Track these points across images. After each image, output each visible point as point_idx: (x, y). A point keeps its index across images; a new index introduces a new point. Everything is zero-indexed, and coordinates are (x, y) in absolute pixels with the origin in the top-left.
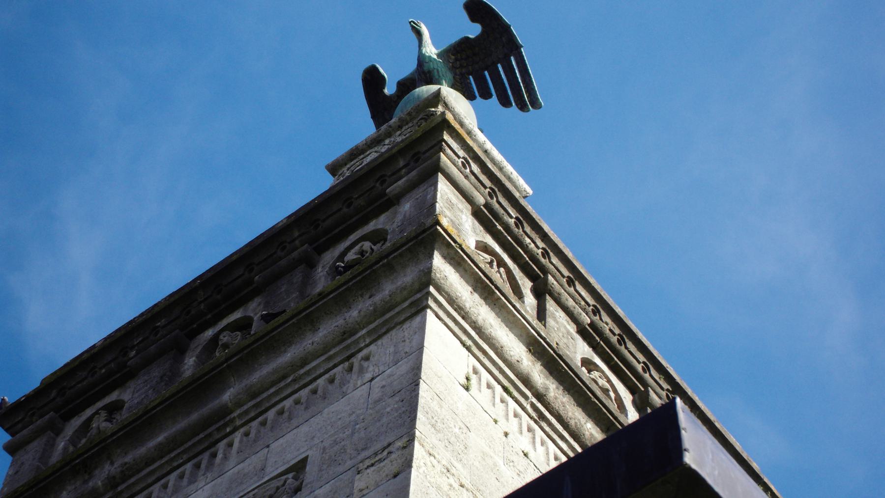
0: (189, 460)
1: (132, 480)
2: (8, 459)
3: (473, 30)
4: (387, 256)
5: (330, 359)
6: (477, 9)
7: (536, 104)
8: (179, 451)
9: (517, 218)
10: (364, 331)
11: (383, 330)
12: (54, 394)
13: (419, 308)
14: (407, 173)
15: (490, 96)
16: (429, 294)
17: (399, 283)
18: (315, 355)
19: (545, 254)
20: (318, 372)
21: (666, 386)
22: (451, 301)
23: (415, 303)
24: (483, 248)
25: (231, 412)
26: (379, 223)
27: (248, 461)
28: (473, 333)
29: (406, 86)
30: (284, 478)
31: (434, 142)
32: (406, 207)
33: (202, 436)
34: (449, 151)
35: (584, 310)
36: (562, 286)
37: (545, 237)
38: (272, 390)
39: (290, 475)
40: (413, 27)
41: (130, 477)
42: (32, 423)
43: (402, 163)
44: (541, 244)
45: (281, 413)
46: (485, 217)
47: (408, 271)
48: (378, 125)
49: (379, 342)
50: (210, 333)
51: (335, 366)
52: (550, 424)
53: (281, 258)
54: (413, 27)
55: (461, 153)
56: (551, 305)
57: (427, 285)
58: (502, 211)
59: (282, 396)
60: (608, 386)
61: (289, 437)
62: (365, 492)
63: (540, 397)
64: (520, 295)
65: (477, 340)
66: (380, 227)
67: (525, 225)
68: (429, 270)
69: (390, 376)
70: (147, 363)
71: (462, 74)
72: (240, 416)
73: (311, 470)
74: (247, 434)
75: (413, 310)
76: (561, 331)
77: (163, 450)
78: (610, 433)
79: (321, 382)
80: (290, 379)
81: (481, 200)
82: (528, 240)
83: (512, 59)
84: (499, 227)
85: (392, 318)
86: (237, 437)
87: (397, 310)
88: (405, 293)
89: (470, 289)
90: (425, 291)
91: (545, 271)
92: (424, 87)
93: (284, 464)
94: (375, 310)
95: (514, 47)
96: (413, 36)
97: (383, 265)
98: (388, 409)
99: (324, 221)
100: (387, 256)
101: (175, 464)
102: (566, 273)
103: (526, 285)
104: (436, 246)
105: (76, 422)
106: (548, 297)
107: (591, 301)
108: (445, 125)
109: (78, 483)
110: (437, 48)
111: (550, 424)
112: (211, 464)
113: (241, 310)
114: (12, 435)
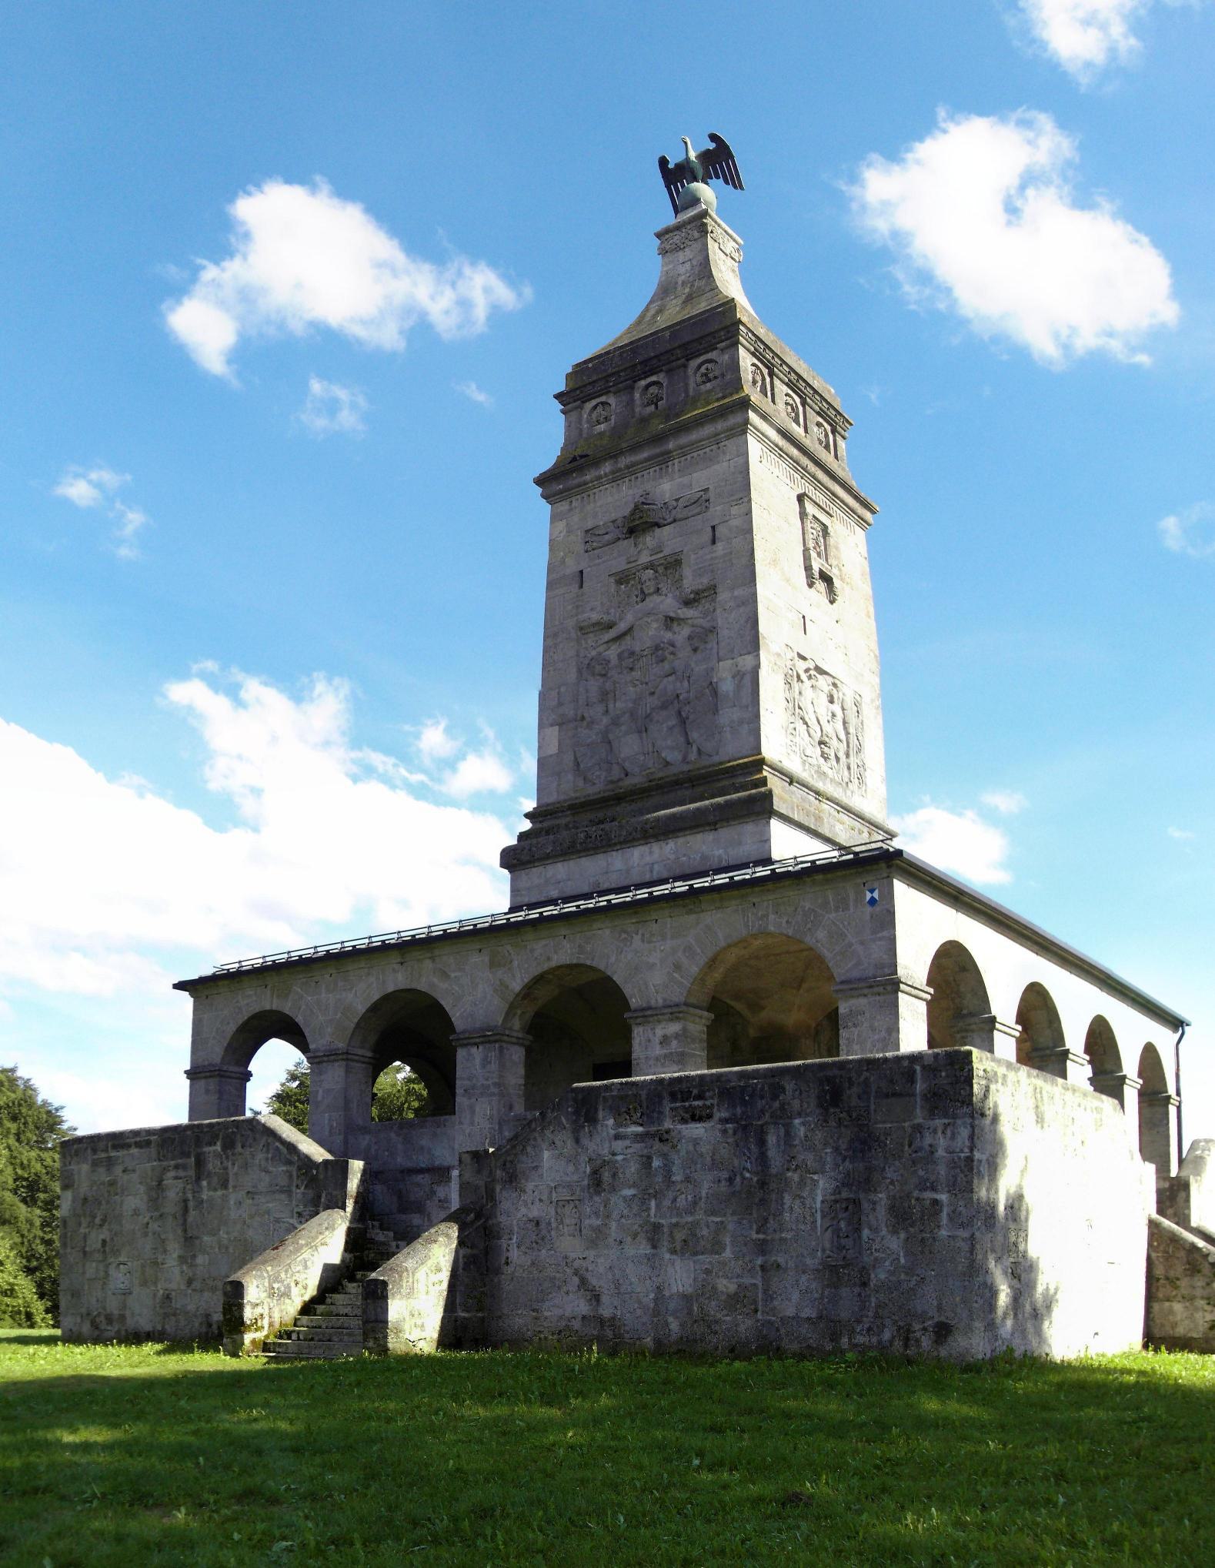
3: (712, 146)
6: (714, 138)
13: (744, 432)
23: (743, 428)
24: (753, 365)
65: (763, 437)
68: (748, 419)
77: (647, 460)
78: (539, 826)
95: (730, 155)
108: (740, 322)
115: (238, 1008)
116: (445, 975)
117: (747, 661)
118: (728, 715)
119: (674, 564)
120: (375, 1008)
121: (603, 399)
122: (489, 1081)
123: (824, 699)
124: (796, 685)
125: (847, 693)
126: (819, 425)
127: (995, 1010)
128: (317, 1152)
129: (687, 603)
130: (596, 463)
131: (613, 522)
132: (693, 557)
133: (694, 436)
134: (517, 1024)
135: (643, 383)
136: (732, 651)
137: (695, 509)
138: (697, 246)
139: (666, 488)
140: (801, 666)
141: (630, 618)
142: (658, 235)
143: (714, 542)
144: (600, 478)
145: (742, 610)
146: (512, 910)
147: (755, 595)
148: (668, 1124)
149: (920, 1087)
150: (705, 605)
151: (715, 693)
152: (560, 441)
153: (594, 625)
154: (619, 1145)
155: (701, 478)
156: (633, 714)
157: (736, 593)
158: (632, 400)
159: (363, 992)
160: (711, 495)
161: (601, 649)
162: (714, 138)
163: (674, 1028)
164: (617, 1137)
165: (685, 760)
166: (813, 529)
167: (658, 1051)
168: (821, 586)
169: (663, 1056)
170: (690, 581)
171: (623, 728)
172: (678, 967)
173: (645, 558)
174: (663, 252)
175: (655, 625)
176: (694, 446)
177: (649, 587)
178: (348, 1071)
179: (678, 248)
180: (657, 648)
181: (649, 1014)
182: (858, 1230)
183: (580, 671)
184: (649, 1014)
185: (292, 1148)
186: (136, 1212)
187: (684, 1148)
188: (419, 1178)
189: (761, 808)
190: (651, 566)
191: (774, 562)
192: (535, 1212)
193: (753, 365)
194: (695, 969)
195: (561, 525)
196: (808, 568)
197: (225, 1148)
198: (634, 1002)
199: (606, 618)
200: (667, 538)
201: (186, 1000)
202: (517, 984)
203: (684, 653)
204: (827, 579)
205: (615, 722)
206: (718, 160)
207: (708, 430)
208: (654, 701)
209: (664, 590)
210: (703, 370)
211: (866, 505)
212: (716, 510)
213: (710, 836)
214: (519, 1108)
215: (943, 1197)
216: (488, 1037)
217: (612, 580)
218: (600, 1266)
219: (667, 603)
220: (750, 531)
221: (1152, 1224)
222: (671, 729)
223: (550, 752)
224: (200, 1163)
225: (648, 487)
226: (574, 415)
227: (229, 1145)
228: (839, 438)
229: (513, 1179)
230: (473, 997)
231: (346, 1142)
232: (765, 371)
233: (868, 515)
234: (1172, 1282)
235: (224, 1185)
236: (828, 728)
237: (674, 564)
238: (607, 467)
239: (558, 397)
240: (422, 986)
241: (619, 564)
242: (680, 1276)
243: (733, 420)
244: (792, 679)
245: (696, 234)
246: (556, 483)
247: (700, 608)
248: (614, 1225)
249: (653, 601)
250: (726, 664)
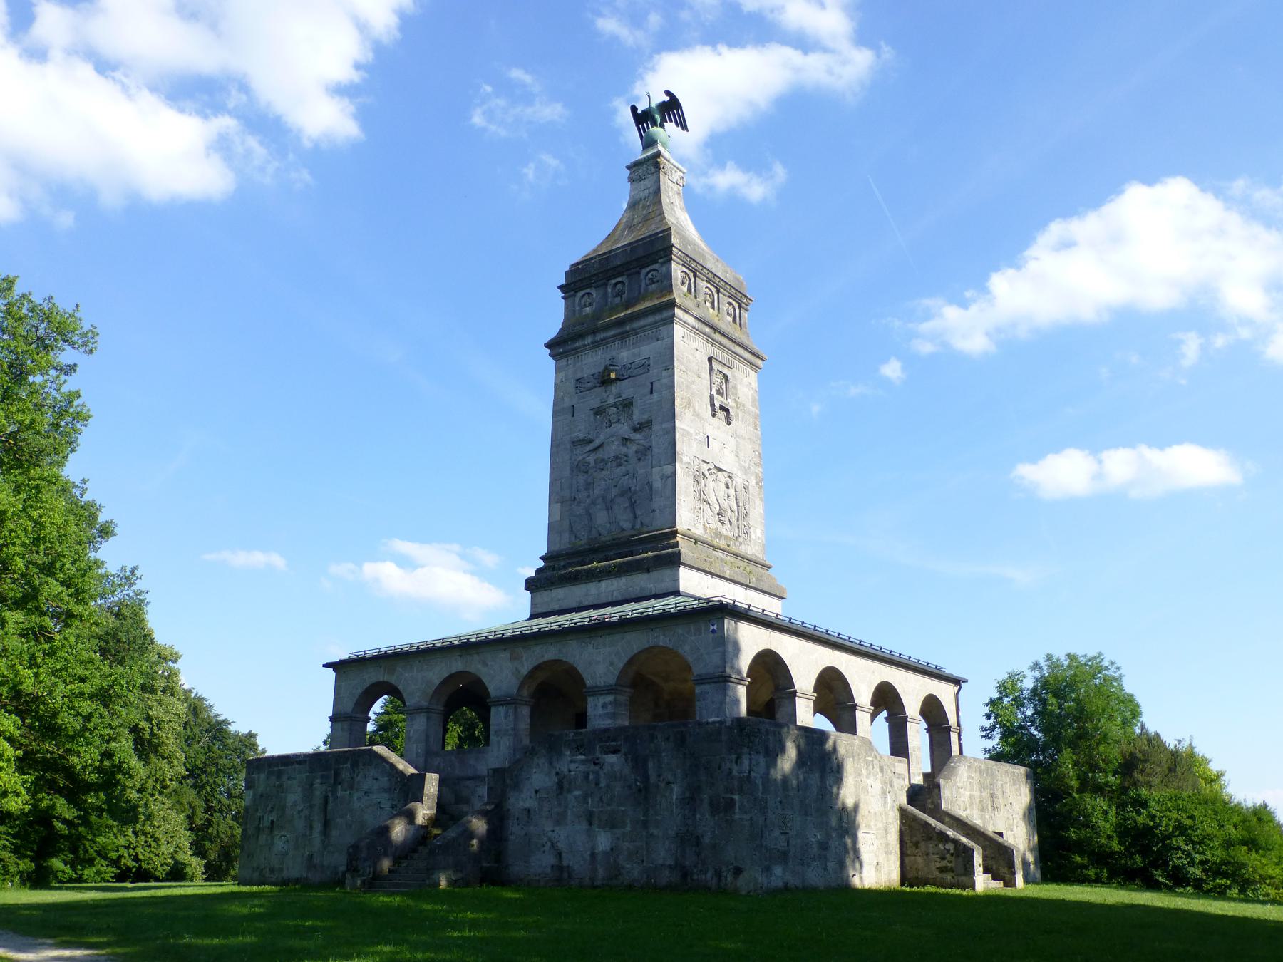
3: (667, 99)
6: (668, 93)
23: (671, 320)
115: (361, 678)
116: (485, 664)
117: (668, 469)
118: (657, 503)
119: (627, 405)
120: (445, 682)
122: (508, 730)
123: (723, 486)
124: (702, 482)
125: (739, 480)
126: (730, 304)
127: (797, 686)
128: (411, 770)
129: (636, 430)
130: (581, 336)
133: (642, 322)
134: (525, 693)
135: (613, 282)
137: (641, 370)
138: (653, 178)
139: (624, 355)
140: (705, 467)
142: (629, 168)
146: (532, 617)
147: (674, 427)
148: (598, 754)
149: (724, 738)
150: (646, 432)
151: (651, 488)
152: (562, 318)
154: (573, 766)
155: (647, 350)
158: (605, 294)
159: (437, 673)
160: (651, 362)
162: (668, 93)
163: (610, 698)
164: (571, 762)
165: (633, 528)
166: (718, 379)
167: (601, 711)
168: (722, 414)
169: (599, 713)
170: (637, 416)
172: (612, 664)
173: (611, 400)
174: (631, 180)
176: (635, 332)
177: (614, 418)
178: (428, 718)
179: (641, 179)
181: (597, 691)
182: (694, 815)
183: (572, 471)
184: (597, 691)
185: (393, 766)
186: (295, 804)
187: (607, 768)
188: (468, 783)
189: (674, 561)
190: (615, 405)
192: (527, 805)
194: (621, 666)
195: (562, 375)
196: (713, 405)
197: (352, 766)
198: (589, 683)
199: (588, 437)
200: (625, 389)
201: (331, 673)
202: (525, 671)
203: (633, 460)
205: (594, 503)
207: (650, 319)
208: (615, 491)
211: (757, 356)
212: (654, 371)
213: (645, 576)
214: (526, 741)
215: (736, 797)
216: (509, 701)
218: (562, 835)
219: (623, 429)
220: (673, 387)
221: (901, 810)
224: (337, 775)
225: (614, 353)
226: (570, 300)
227: (355, 765)
229: (517, 787)
230: (500, 677)
231: (426, 761)
232: (691, 275)
233: (759, 363)
234: (916, 845)
235: (351, 788)
236: (725, 505)
237: (627, 405)
238: (589, 340)
239: (560, 287)
240: (472, 669)
241: (596, 403)
242: (603, 841)
243: (666, 314)
244: (698, 478)
245: (653, 170)
246: (558, 346)
248: (569, 812)
249: (616, 427)
250: (656, 470)
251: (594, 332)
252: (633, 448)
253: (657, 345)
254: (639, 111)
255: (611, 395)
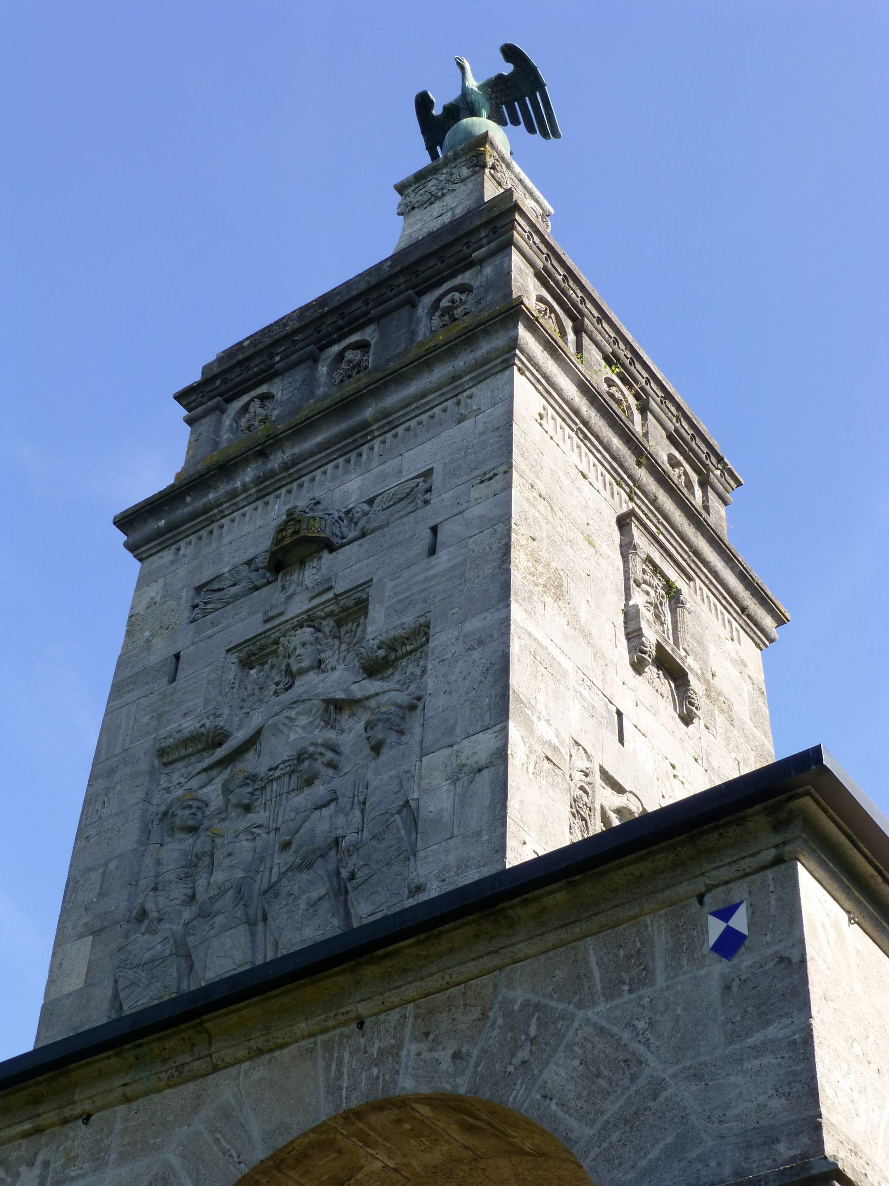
0: (341, 456)
1: (300, 466)
2: (188, 429)
3: (507, 69)
4: (484, 324)
5: (443, 394)
6: (511, 53)
7: (556, 134)
8: (333, 449)
9: (564, 275)
10: (468, 377)
11: (482, 378)
12: (218, 382)
13: (508, 365)
14: (489, 243)
15: (519, 123)
16: (515, 355)
17: (494, 345)
18: (432, 391)
19: (583, 301)
20: (435, 404)
21: (660, 394)
22: (530, 359)
23: (506, 359)
24: (540, 299)
25: (371, 425)
26: (465, 278)
27: (387, 464)
28: (543, 381)
29: (454, 112)
30: (417, 480)
31: (508, 221)
32: (488, 270)
33: (350, 440)
34: (519, 228)
35: (607, 341)
36: (592, 324)
37: (583, 288)
38: (400, 413)
39: (421, 479)
40: (458, 63)
41: (298, 464)
42: (202, 404)
43: (483, 234)
44: (580, 294)
45: (408, 429)
46: (542, 277)
47: (499, 335)
48: (431, 149)
49: (479, 386)
50: (336, 349)
51: (446, 400)
52: (591, 442)
53: (390, 299)
54: (458, 63)
55: (527, 229)
56: (586, 340)
57: (514, 348)
58: (554, 271)
59: (409, 417)
60: (621, 397)
61: (417, 450)
62: (479, 501)
63: (585, 423)
64: (563, 333)
65: (546, 385)
66: (466, 281)
67: (570, 280)
68: (516, 338)
69: (490, 415)
70: (291, 367)
71: (497, 104)
72: (378, 429)
73: (437, 479)
74: (384, 442)
75: (504, 365)
76: (600, 373)
77: (322, 447)
79: (437, 410)
80: (413, 406)
81: (540, 265)
82: (571, 292)
83: (538, 94)
84: (552, 283)
85: (489, 370)
86: (376, 443)
87: (492, 364)
88: (498, 353)
89: (541, 348)
90: (513, 353)
91: (582, 314)
92: (469, 119)
93: (416, 470)
94: (476, 363)
95: (539, 85)
96: (458, 69)
97: (482, 330)
98: (491, 441)
99: (423, 272)
100: (484, 324)
101: (331, 458)
102: (596, 314)
103: (568, 324)
104: (520, 319)
105: (237, 404)
106: (584, 334)
107: (613, 334)
109: (259, 464)
110: (477, 81)
111: (591, 442)
112: (358, 462)
113: (360, 333)
114: (189, 410)
117: (482, 746)
121: (263, 389)
129: (373, 669)
131: (249, 563)
132: (390, 585)
133: (413, 388)
136: (451, 731)
139: (345, 487)
141: (257, 719)
142: (401, 188)
143: (432, 551)
144: (234, 494)
145: (476, 654)
147: (506, 622)
152: (182, 464)
153: (187, 742)
156: (240, 891)
157: (468, 627)
161: (194, 783)
162: (511, 53)
170: (379, 625)
171: (219, 920)
173: (299, 606)
175: (303, 720)
176: (388, 422)
180: (301, 757)
183: (146, 831)
190: (310, 620)
191: (557, 588)
193: (540, 299)
196: (633, 635)
200: (345, 568)
204: (675, 673)
206: (518, 91)
207: (441, 372)
208: (281, 861)
209: (332, 662)
210: (445, 303)
211: (764, 600)
212: (443, 498)
217: (233, 658)
222: (313, 905)
223: (67, 989)
228: (711, 495)
237: (352, 609)
238: (249, 474)
247: (397, 677)
251: (262, 452)
252: (352, 731)
253: (455, 435)
254: (437, 111)
255: (298, 594)
